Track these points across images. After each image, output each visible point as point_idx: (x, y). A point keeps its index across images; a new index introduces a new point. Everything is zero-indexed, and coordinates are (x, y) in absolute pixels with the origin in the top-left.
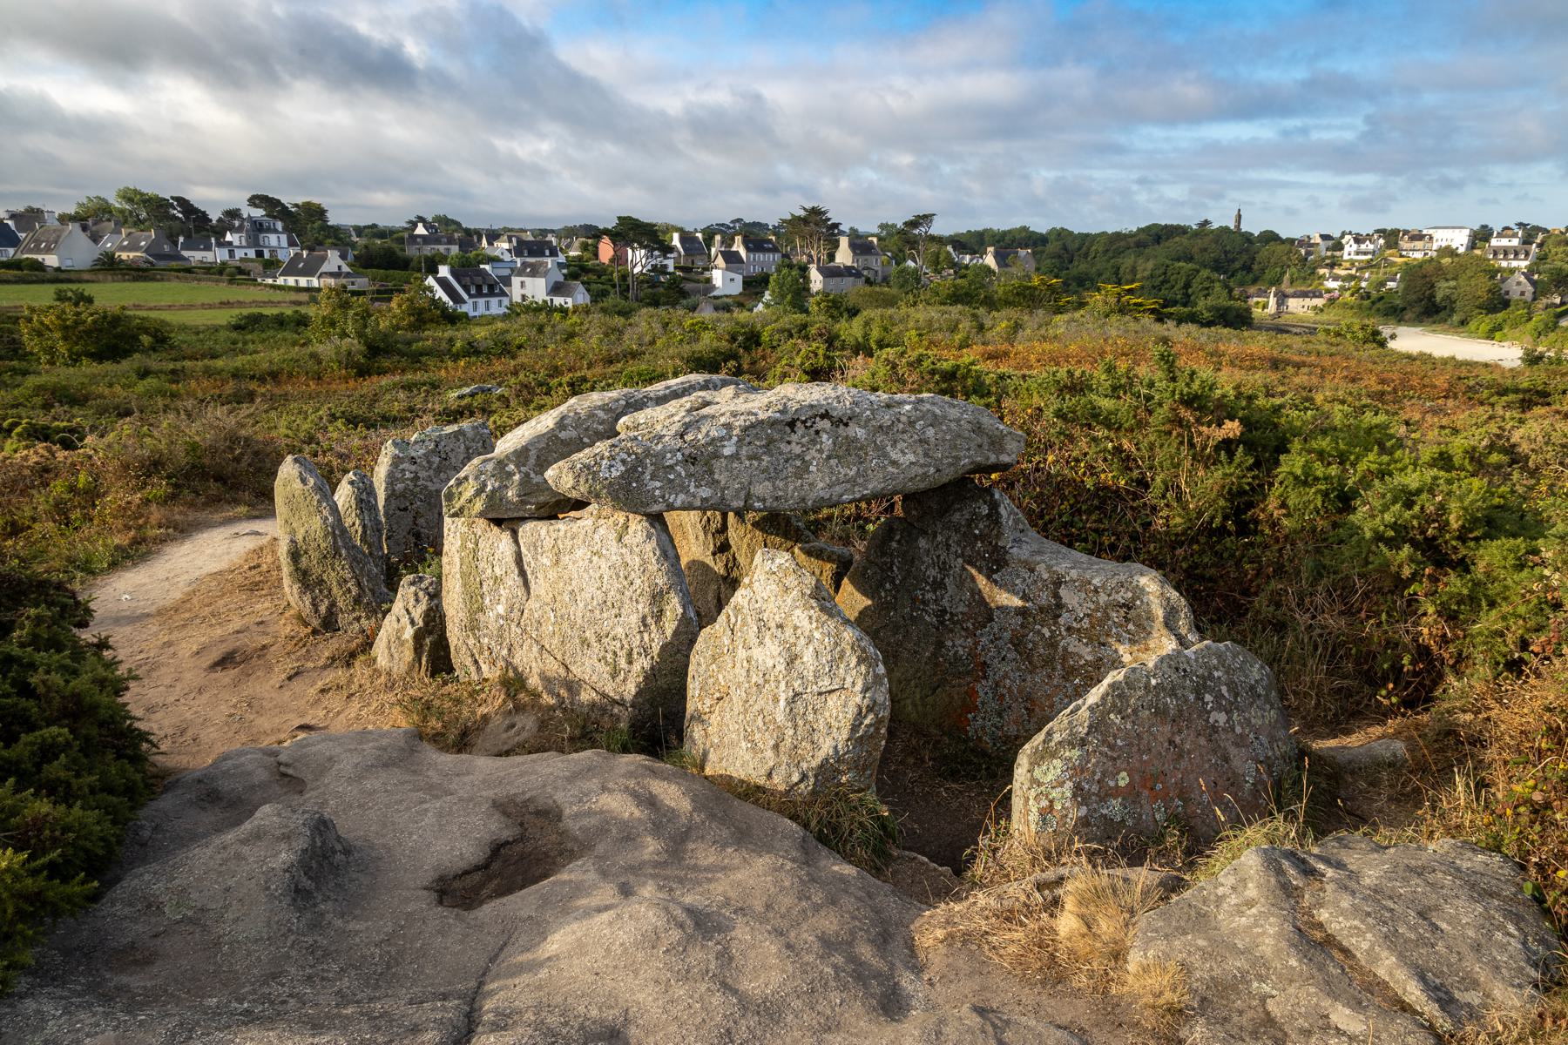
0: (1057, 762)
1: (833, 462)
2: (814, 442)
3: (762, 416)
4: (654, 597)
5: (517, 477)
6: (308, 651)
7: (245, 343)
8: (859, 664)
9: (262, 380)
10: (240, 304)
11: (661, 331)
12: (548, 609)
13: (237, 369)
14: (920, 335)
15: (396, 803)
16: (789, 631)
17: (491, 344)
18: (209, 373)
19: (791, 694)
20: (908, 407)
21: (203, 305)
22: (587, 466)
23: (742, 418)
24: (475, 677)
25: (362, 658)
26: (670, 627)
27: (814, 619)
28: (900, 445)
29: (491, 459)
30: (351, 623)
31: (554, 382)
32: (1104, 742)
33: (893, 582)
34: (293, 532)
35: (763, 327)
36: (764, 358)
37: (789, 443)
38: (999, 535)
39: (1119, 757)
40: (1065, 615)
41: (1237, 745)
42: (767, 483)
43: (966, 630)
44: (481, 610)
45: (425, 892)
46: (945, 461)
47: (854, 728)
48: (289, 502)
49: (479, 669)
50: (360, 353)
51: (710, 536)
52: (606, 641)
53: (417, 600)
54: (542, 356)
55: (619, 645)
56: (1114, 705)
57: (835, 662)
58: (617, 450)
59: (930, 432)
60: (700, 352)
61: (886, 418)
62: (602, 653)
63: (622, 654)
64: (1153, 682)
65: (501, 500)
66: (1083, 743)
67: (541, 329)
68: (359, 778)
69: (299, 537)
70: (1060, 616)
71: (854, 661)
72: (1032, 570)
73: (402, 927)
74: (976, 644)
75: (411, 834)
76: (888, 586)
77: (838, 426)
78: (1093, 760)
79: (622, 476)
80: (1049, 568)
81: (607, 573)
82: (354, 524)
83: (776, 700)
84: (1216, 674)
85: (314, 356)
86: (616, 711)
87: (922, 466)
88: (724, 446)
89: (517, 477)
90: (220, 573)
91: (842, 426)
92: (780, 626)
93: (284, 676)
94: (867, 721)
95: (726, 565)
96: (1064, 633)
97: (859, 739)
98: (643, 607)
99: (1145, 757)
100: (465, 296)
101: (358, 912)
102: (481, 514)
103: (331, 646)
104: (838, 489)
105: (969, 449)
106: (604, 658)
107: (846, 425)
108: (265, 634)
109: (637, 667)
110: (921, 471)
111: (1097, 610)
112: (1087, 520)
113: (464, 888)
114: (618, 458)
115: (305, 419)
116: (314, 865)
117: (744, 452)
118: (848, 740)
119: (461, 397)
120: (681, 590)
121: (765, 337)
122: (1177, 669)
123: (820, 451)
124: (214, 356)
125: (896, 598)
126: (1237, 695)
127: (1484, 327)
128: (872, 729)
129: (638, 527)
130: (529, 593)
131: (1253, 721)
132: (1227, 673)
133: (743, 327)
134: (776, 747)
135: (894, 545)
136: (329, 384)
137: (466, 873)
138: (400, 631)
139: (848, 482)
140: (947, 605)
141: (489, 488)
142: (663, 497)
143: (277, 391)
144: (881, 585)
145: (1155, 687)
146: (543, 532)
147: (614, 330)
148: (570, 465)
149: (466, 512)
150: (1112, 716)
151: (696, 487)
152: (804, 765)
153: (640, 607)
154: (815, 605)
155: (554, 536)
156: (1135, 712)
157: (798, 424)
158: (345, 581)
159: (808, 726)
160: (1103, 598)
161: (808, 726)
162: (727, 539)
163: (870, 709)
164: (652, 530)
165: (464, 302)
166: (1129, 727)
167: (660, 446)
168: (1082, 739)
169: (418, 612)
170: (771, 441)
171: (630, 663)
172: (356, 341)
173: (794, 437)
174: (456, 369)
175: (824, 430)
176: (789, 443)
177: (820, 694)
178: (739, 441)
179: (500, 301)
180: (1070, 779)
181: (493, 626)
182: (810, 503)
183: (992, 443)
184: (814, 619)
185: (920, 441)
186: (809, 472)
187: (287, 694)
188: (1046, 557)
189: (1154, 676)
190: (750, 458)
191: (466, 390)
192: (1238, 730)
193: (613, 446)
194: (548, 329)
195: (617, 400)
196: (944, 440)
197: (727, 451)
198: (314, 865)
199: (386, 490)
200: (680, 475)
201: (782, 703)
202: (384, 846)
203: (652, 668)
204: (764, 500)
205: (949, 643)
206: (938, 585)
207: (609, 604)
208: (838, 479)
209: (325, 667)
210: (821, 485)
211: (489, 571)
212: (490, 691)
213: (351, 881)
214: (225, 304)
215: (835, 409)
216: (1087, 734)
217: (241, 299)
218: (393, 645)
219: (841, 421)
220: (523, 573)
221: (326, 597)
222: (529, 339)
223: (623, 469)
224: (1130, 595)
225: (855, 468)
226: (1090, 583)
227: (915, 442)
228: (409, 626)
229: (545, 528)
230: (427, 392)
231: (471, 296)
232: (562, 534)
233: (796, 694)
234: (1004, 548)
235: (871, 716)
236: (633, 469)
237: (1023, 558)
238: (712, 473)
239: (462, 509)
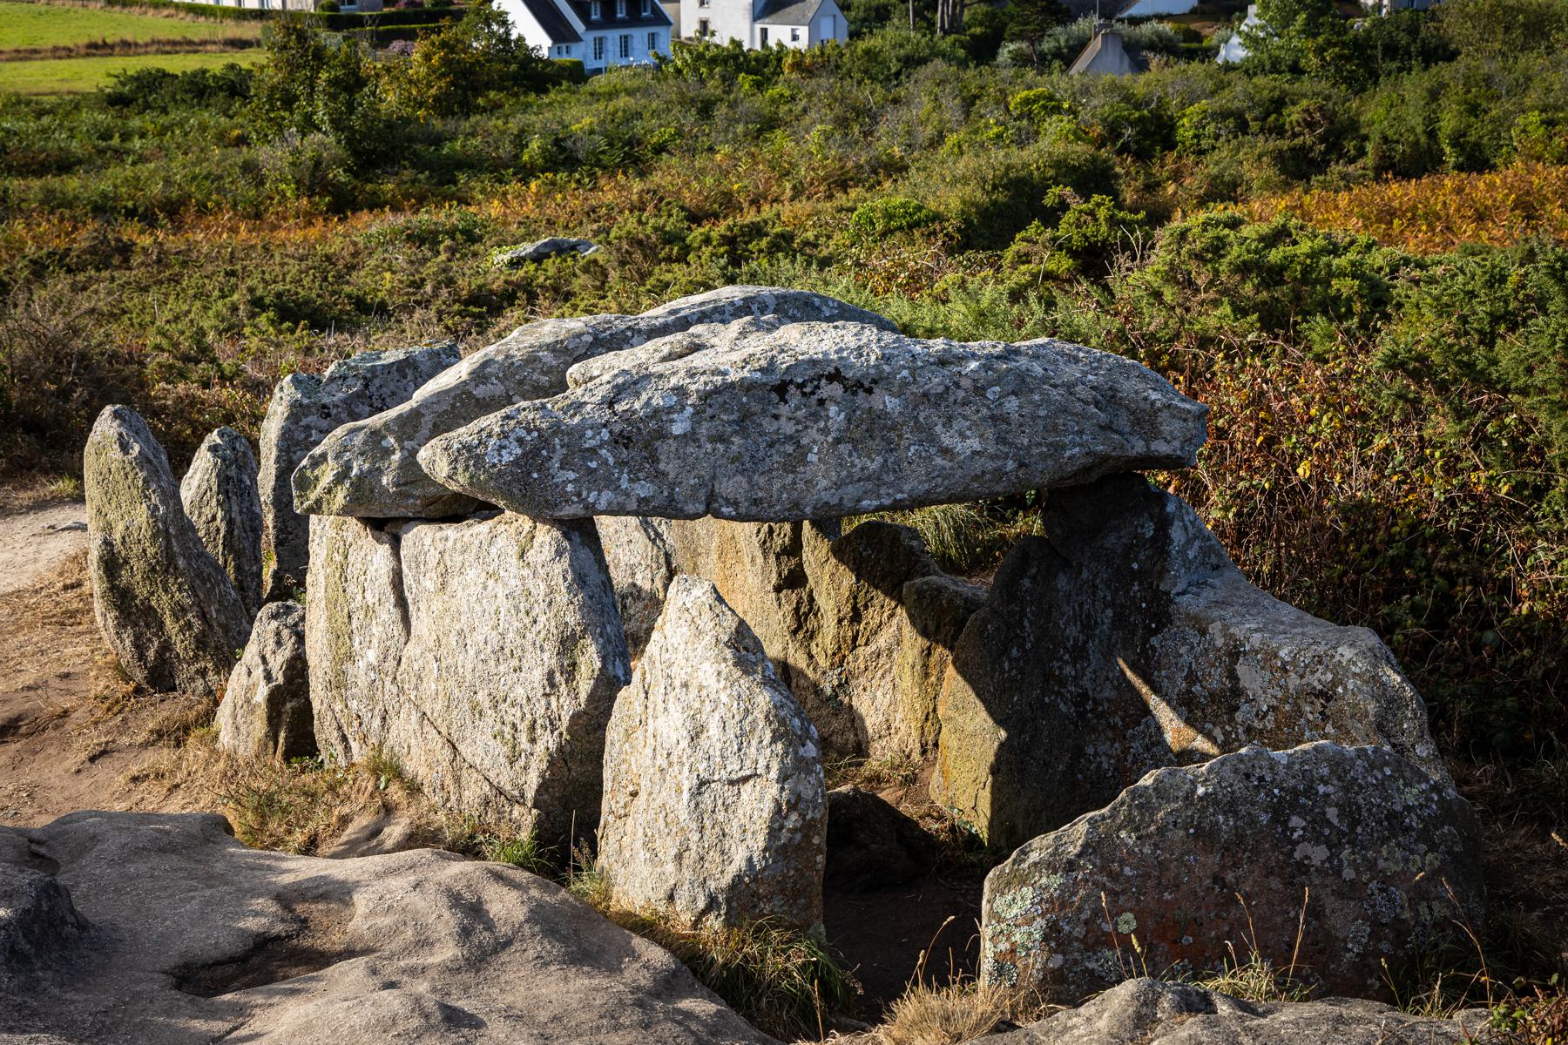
0: (1028, 891)
1: (844, 448)
2: (815, 417)
3: (733, 377)
4: (562, 643)
5: (397, 457)
6: (125, 720)
7: (126, 137)
8: (774, 741)
9: (149, 220)
10: (127, 47)
11: (959, 116)
12: (430, 657)
13: (104, 195)
14: (1550, 123)
15: (160, 889)
16: (693, 691)
17: (602, 143)
18: (53, 203)
19: (695, 782)
20: (973, 365)
21: (55, 49)
22: (467, 447)
23: (703, 379)
24: (342, 762)
25: (199, 732)
26: (585, 687)
27: (724, 675)
28: (959, 424)
29: (363, 428)
30: (192, 679)
31: (697, 234)
32: (1102, 869)
33: (1021, 646)
34: (108, 528)
35: (1182, 106)
36: (1177, 176)
37: (776, 417)
38: (1163, 572)
39: (1124, 892)
40: (1245, 707)
41: (1339, 894)
42: (739, 478)
43: (1113, 727)
44: (350, 657)
45: (163, 976)
46: (1035, 451)
47: (773, 833)
48: (103, 480)
49: (347, 749)
50: (341, 163)
51: (772, 558)
52: (503, 706)
53: (279, 643)
54: (703, 171)
55: (519, 714)
56: (1129, 819)
57: (743, 736)
58: (512, 423)
59: (1012, 404)
60: (1026, 165)
61: (935, 381)
62: (498, 726)
63: (523, 727)
64: (1201, 791)
65: (372, 491)
66: (1071, 866)
67: (706, 110)
68: (125, 861)
69: (117, 537)
70: (1237, 708)
71: (768, 736)
72: (1203, 632)
73: (125, 1004)
74: (1126, 751)
75: (165, 919)
76: (1014, 651)
77: (855, 393)
78: (1082, 892)
79: (515, 463)
80: (1226, 628)
81: (505, 605)
82: (214, 518)
83: (679, 791)
84: (1322, 789)
85: (249, 168)
86: (516, 814)
87: (992, 457)
88: (673, 421)
89: (397, 457)
90: (18, 593)
91: (861, 394)
92: (685, 685)
93: (83, 756)
94: (790, 824)
95: (797, 610)
96: (1243, 737)
97: (781, 846)
98: (549, 659)
99: (1167, 896)
100: (579, 26)
101: (81, 985)
102: (345, 511)
103: (167, 710)
104: (851, 491)
105: (1081, 432)
106: (501, 733)
107: (870, 391)
108: (69, 693)
109: (540, 748)
110: (990, 465)
111: (1285, 700)
112: (1435, 554)
113: (212, 979)
114: (512, 436)
115: (206, 308)
116: (36, 929)
117: (704, 430)
118: (765, 850)
119: (516, 263)
120: (601, 635)
121: (1185, 131)
122: (1248, 776)
123: (825, 431)
124: (65, 165)
125: (1022, 673)
126: (1355, 823)
128: (798, 836)
129: (546, 537)
130: (409, 633)
131: (1381, 864)
132: (1347, 790)
133: (1137, 107)
134: (679, 857)
135: (1027, 583)
136: (274, 228)
137: (218, 963)
138: (250, 689)
139: (868, 479)
140: (1089, 685)
141: (355, 471)
142: (579, 495)
143: (174, 243)
144: (1005, 651)
145: (1201, 798)
146: (428, 541)
147: (860, 112)
148: (445, 444)
149: (325, 506)
150: (1123, 834)
151: (631, 480)
152: (712, 885)
153: (546, 656)
154: (729, 656)
155: (440, 547)
156: (1161, 831)
157: (792, 389)
158: (184, 610)
159: (717, 829)
160: (1293, 681)
161: (717, 829)
162: (800, 565)
163: (792, 807)
164: (566, 544)
165: (576, 38)
166: (1147, 850)
167: (577, 419)
168: (1070, 862)
169: (278, 662)
170: (746, 415)
171: (533, 741)
172: (332, 139)
173: (784, 410)
174: (521, 198)
175: (832, 399)
176: (776, 417)
177: (732, 783)
178: (696, 413)
179: (652, 37)
180: (1043, 915)
181: (363, 682)
183: (1137, 422)
184: (724, 675)
185: (993, 418)
186: (806, 463)
187: (85, 783)
188: (1228, 613)
189: (1204, 783)
190: (714, 439)
191: (527, 248)
192: (1348, 874)
193: (508, 417)
194: (721, 111)
195: (580, 335)
196: (1034, 417)
197: (677, 429)
198: (36, 929)
199: (277, 461)
200: (606, 462)
201: (686, 796)
202: (130, 930)
203: (560, 749)
204: (736, 504)
205: (1090, 750)
206: (1080, 653)
207: (507, 651)
208: (850, 475)
209: (145, 745)
210: (824, 483)
211: (359, 597)
212: (355, 780)
213: (81, 957)
214: (98, 49)
215: (852, 366)
216: (1079, 856)
217: (129, 38)
218: (240, 712)
219: (861, 385)
220: (402, 603)
221: (155, 635)
222: (679, 133)
223: (519, 451)
224: (1330, 676)
225: (879, 459)
226: (1276, 656)
227: (984, 419)
228: (263, 683)
229: (430, 534)
230: (452, 251)
231: (590, 25)
232: (450, 544)
234: (1168, 593)
235: (794, 817)
236: (535, 452)
237: (1193, 610)
238: (655, 460)
239: (319, 502)
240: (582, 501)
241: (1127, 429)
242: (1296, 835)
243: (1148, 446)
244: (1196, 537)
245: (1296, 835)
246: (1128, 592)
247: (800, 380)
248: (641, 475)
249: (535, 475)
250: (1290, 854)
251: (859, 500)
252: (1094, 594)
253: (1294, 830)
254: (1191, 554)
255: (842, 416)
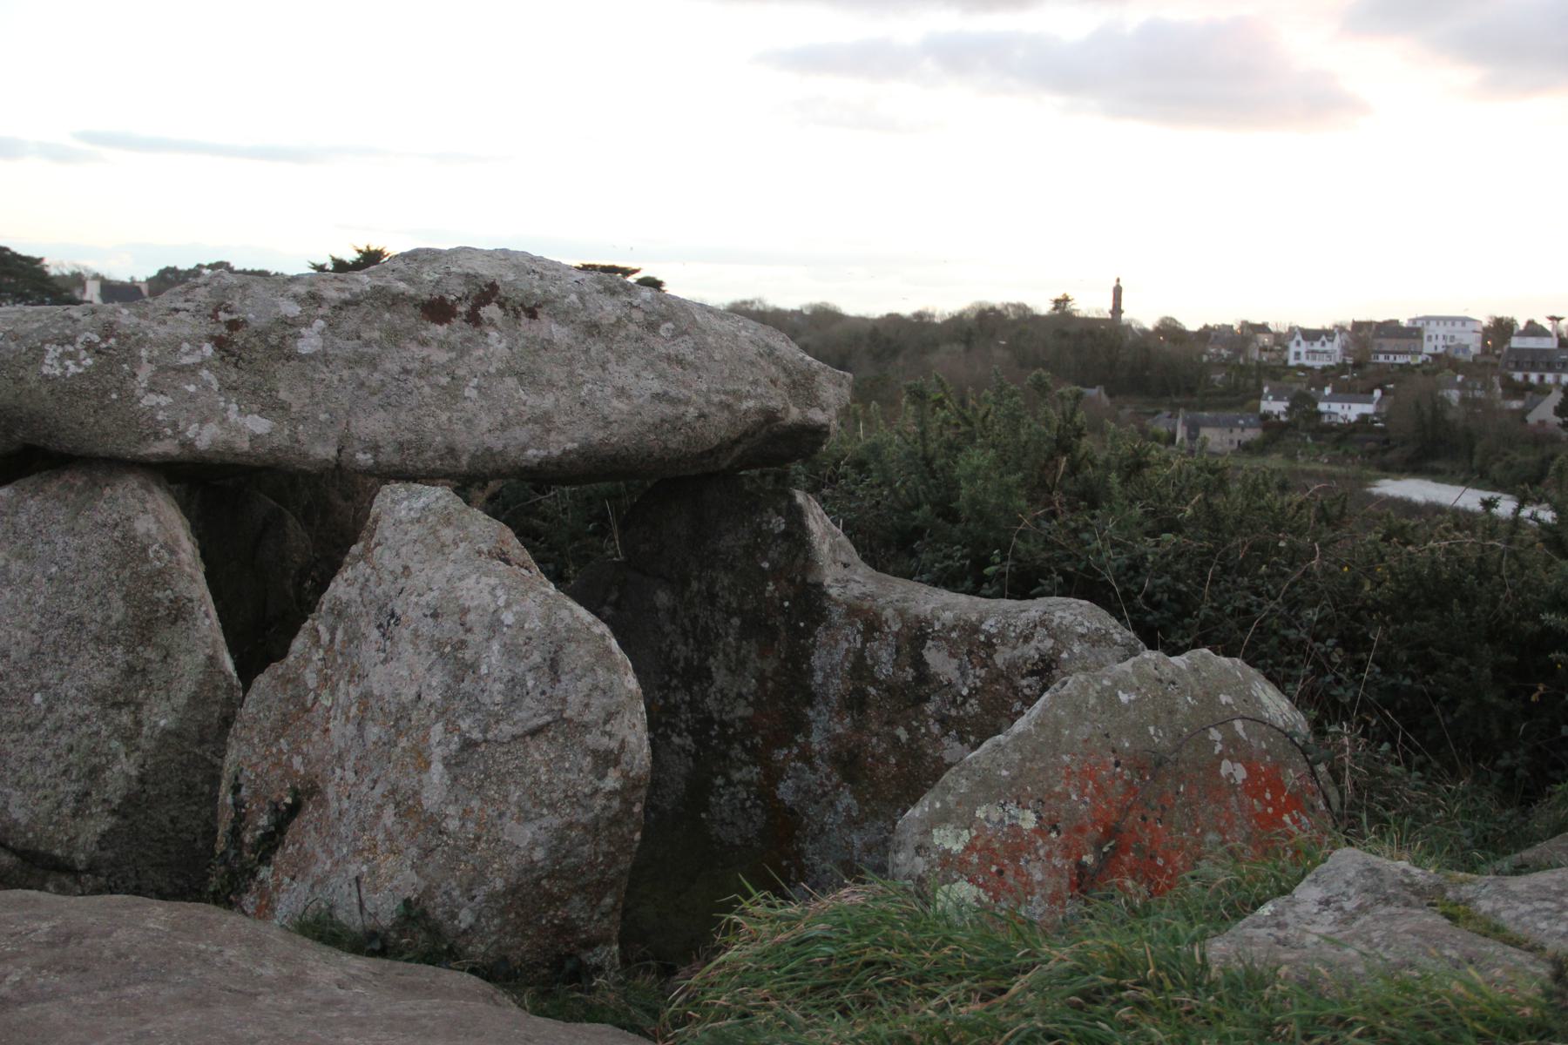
42: (381, 414)
127: (1462, 477)
182: (465, 460)
233: (469, 745)
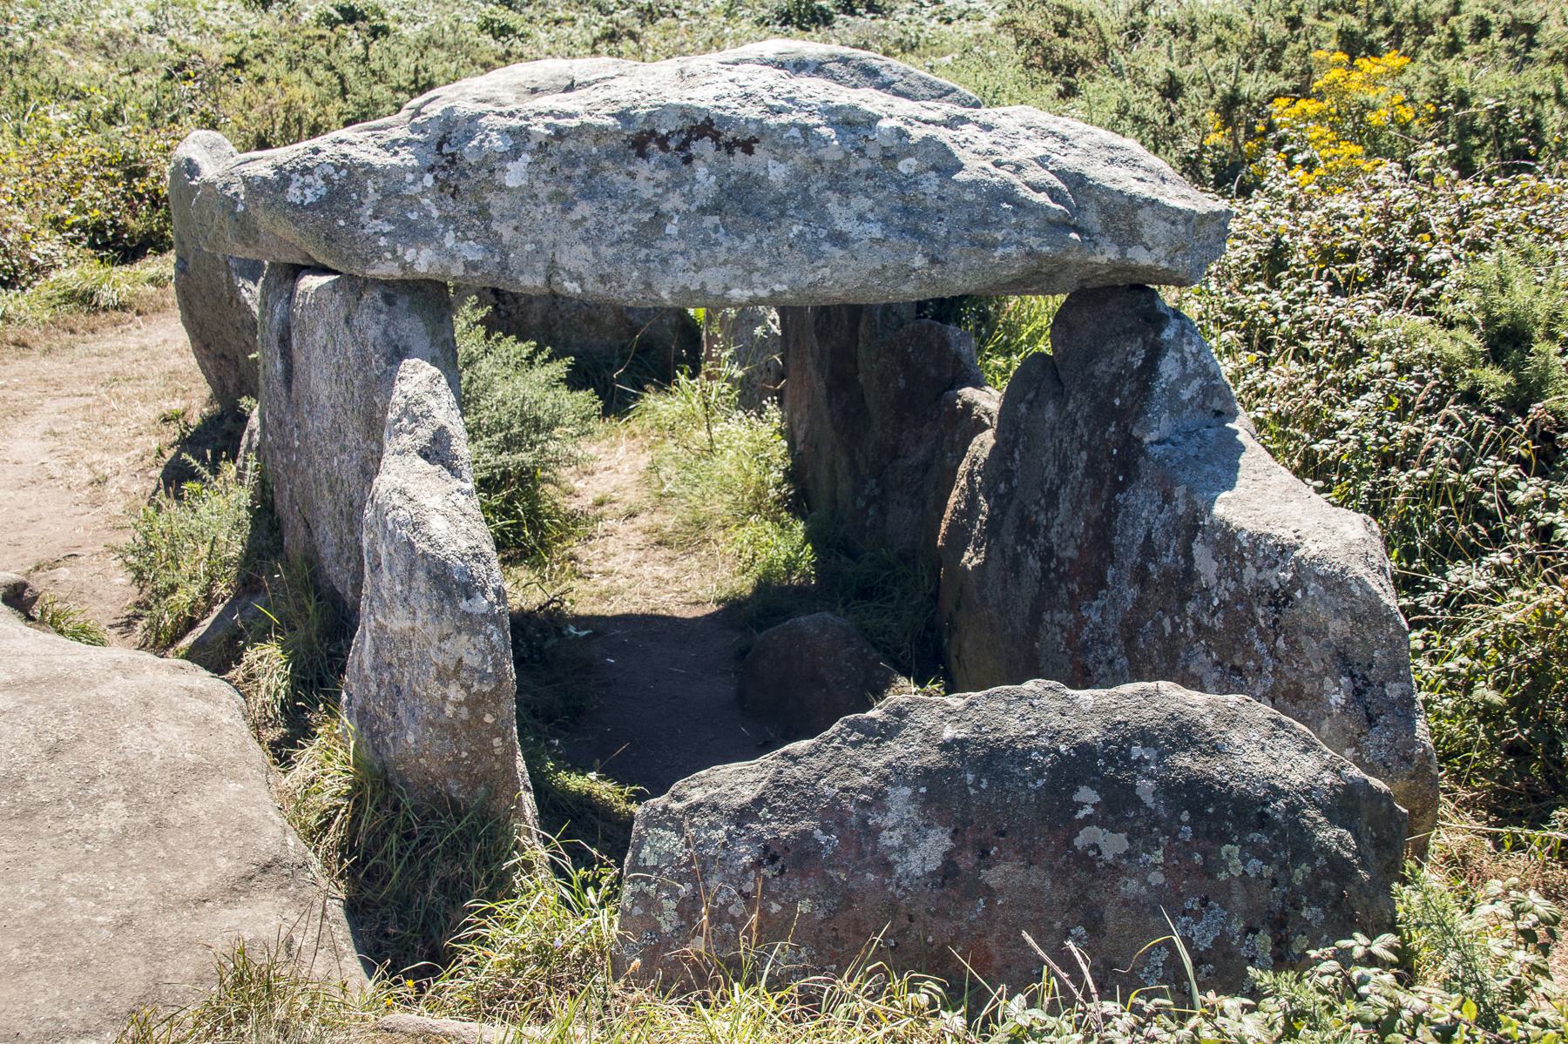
77: (730, 153)
142: (394, 252)
205: (1047, 617)
225: (751, 238)
240: (396, 258)
241: (1098, 228)
242: (1081, 814)
243: (1123, 253)
244: (1196, 374)
245: (1081, 814)
246: (1103, 433)
247: (664, 132)
248: (470, 234)
249: (342, 223)
250: (1068, 843)
251: (727, 288)
252: (1073, 430)
253: (1081, 805)
254: (1186, 395)
255: (713, 178)
